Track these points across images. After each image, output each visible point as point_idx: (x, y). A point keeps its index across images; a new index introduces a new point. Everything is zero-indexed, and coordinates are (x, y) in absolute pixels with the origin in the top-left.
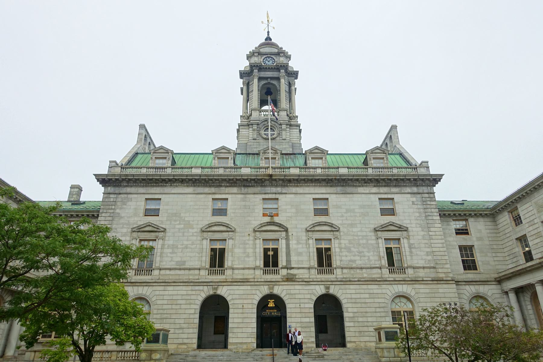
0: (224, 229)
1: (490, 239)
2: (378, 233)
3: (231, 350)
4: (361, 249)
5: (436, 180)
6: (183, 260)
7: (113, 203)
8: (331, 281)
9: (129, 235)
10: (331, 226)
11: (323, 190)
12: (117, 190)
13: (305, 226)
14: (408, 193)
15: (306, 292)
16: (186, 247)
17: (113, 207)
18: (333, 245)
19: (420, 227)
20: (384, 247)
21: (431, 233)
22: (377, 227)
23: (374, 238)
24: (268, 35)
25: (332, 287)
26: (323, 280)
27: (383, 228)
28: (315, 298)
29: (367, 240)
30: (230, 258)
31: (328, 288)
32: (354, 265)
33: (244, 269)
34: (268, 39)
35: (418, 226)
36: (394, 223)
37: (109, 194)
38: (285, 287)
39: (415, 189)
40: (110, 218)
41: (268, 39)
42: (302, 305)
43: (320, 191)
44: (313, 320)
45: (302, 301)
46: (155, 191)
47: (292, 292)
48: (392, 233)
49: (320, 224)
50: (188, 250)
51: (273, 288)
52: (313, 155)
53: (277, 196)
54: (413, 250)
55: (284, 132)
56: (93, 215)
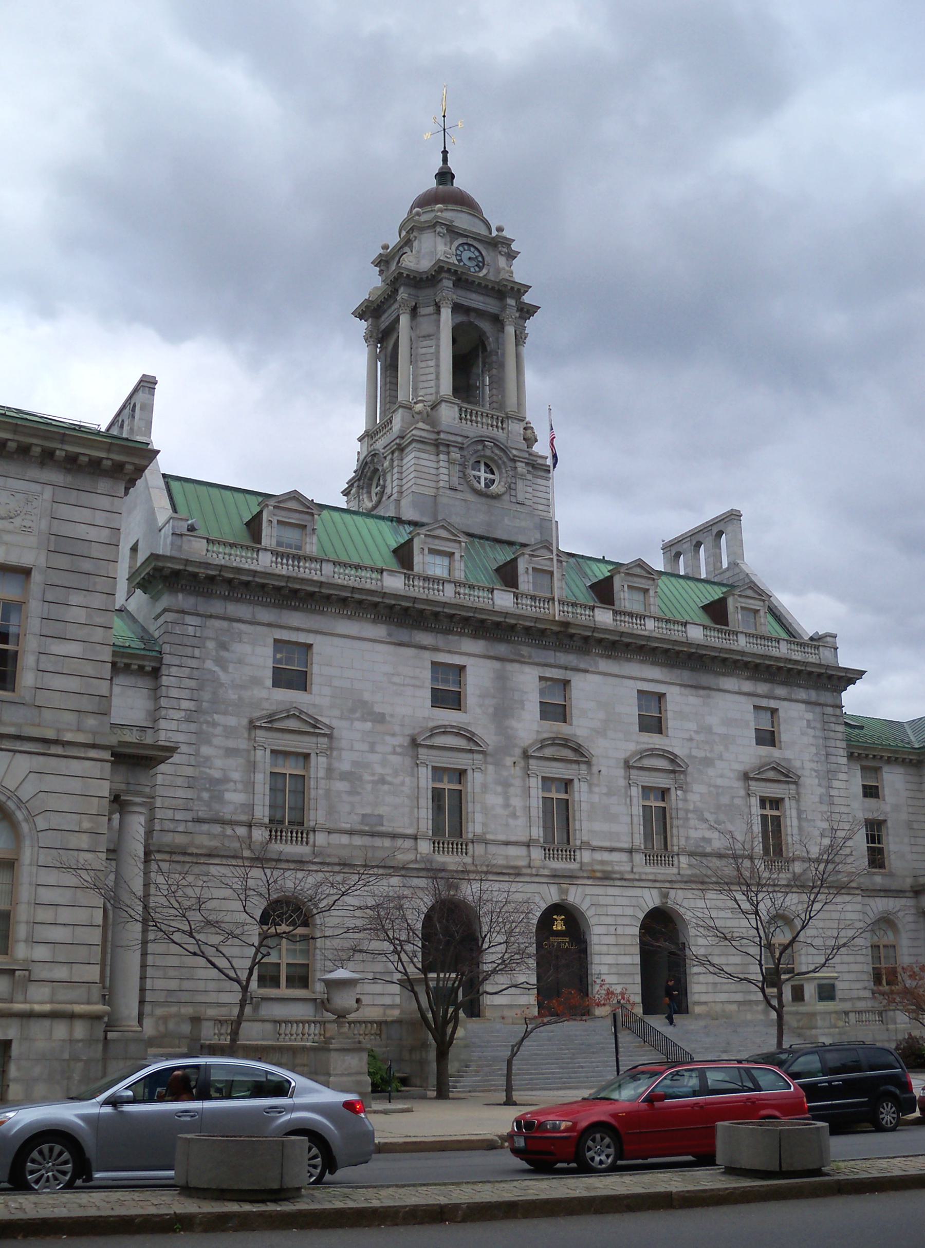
0: (461, 743)
1: (910, 810)
2: (751, 783)
3: (699, 1016)
4: (722, 817)
5: (851, 677)
6: (376, 813)
7: (195, 641)
8: (670, 882)
9: (246, 735)
10: (470, 739)
11: (655, 672)
12: (204, 606)
13: (622, 755)
14: (803, 702)
15: (625, 901)
16: (382, 781)
17: (197, 652)
18: (312, 771)
19: (816, 777)
20: (540, 796)
21: (833, 792)
22: (259, 719)
23: (742, 793)
24: (445, 160)
25: (672, 893)
26: (660, 878)
27: (271, 722)
28: (641, 916)
29: (733, 798)
30: (479, 817)
31: (665, 896)
32: (708, 850)
33: (507, 843)
34: (445, 176)
35: (814, 774)
36: (301, 712)
37: (183, 612)
38: (589, 890)
39: (813, 695)
40: (192, 684)
41: (445, 176)
42: (620, 930)
43: (651, 676)
44: (637, 959)
45: (620, 921)
46: (298, 624)
47: (603, 900)
48: (772, 785)
49: (444, 731)
50: (386, 787)
51: (566, 892)
52: (283, 513)
53: (569, 675)
54: (804, 824)
55: (520, 484)
56: (141, 668)
